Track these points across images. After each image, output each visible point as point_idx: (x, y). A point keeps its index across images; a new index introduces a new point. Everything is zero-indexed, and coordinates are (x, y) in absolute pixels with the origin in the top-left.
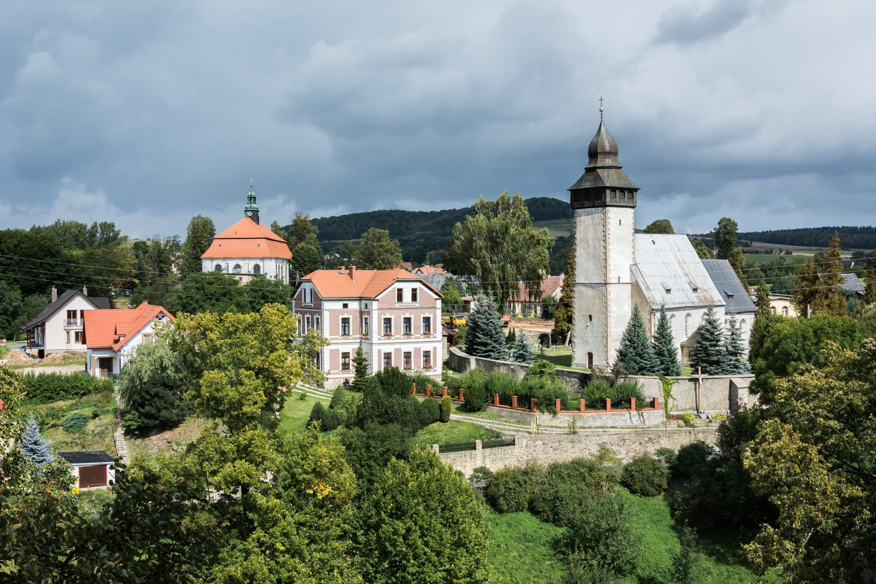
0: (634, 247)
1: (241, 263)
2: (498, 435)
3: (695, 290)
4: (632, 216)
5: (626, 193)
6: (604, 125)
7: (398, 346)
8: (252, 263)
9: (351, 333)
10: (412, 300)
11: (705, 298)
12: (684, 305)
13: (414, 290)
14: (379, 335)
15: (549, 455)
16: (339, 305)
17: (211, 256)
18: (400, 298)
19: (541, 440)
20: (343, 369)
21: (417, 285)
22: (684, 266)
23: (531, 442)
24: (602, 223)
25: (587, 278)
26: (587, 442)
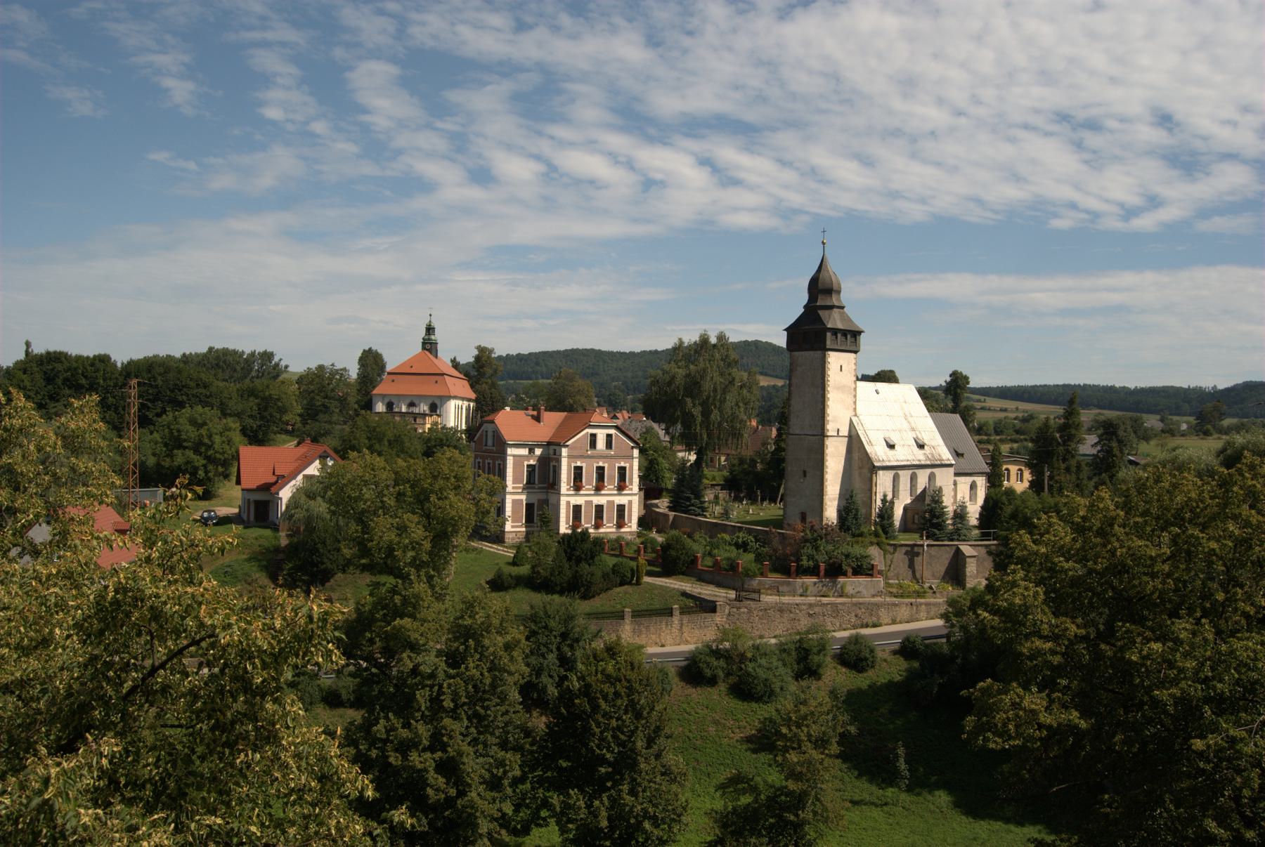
0: (855, 396)
10: (607, 448)
12: (909, 463)
13: (609, 436)
16: (524, 452)
18: (593, 444)
21: (612, 431)
22: (910, 419)
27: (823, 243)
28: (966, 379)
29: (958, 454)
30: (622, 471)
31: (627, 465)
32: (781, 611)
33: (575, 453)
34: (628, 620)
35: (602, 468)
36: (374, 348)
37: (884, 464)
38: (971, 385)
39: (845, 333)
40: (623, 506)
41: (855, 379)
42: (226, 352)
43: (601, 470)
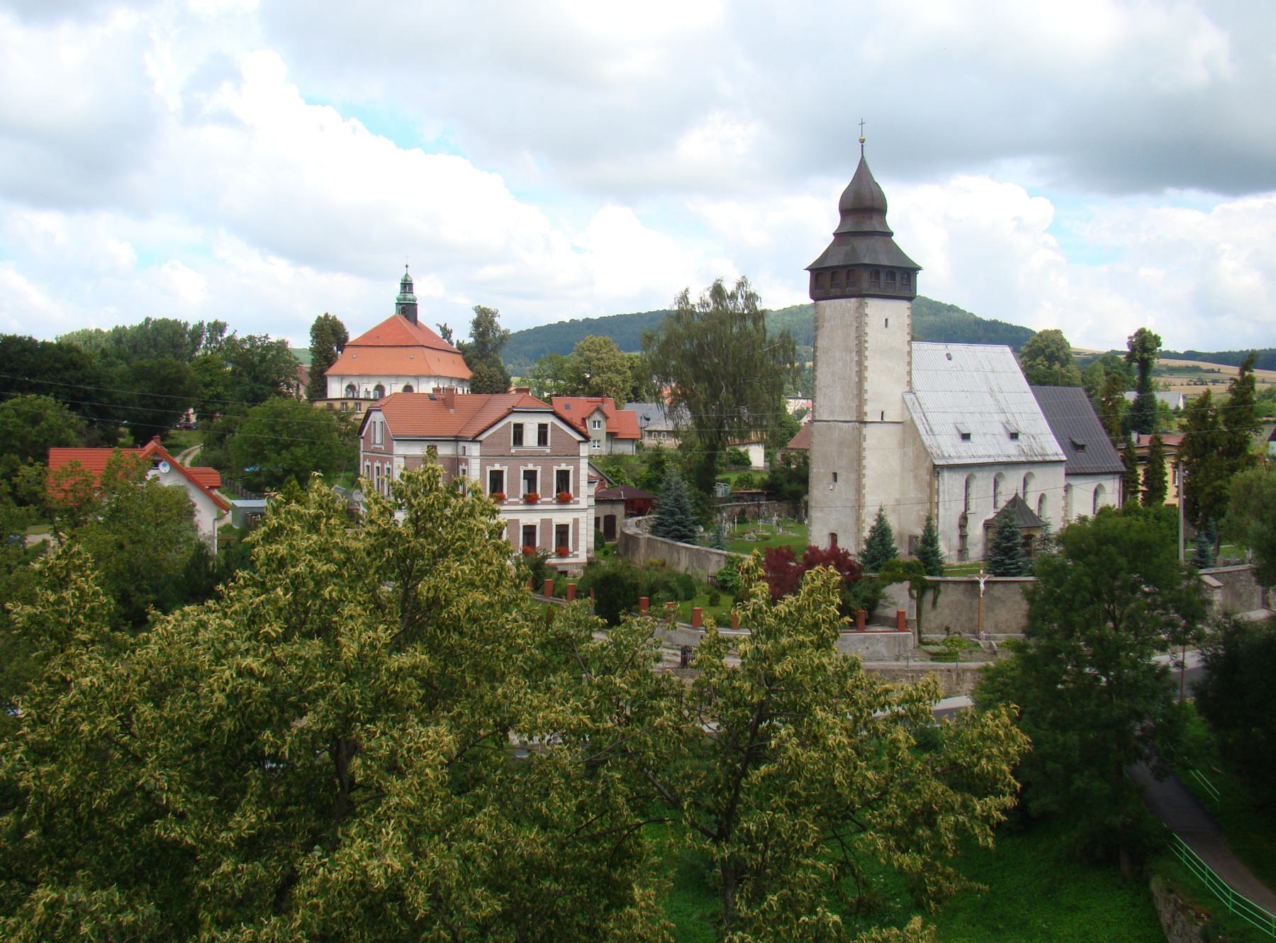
0: (910, 364)
1: (413, 383)
3: (1014, 436)
4: (908, 312)
7: (546, 516)
10: (539, 443)
11: (1031, 449)
12: (991, 460)
13: (542, 428)
16: (419, 450)
17: (366, 372)
18: (518, 439)
21: (549, 420)
22: (999, 396)
24: (855, 324)
25: (832, 412)
27: (862, 141)
28: (1157, 340)
29: (1075, 447)
30: (563, 477)
31: (571, 468)
33: (491, 451)
36: (331, 314)
37: (951, 462)
38: (1163, 348)
40: (533, 527)
41: (909, 338)
42: (165, 324)
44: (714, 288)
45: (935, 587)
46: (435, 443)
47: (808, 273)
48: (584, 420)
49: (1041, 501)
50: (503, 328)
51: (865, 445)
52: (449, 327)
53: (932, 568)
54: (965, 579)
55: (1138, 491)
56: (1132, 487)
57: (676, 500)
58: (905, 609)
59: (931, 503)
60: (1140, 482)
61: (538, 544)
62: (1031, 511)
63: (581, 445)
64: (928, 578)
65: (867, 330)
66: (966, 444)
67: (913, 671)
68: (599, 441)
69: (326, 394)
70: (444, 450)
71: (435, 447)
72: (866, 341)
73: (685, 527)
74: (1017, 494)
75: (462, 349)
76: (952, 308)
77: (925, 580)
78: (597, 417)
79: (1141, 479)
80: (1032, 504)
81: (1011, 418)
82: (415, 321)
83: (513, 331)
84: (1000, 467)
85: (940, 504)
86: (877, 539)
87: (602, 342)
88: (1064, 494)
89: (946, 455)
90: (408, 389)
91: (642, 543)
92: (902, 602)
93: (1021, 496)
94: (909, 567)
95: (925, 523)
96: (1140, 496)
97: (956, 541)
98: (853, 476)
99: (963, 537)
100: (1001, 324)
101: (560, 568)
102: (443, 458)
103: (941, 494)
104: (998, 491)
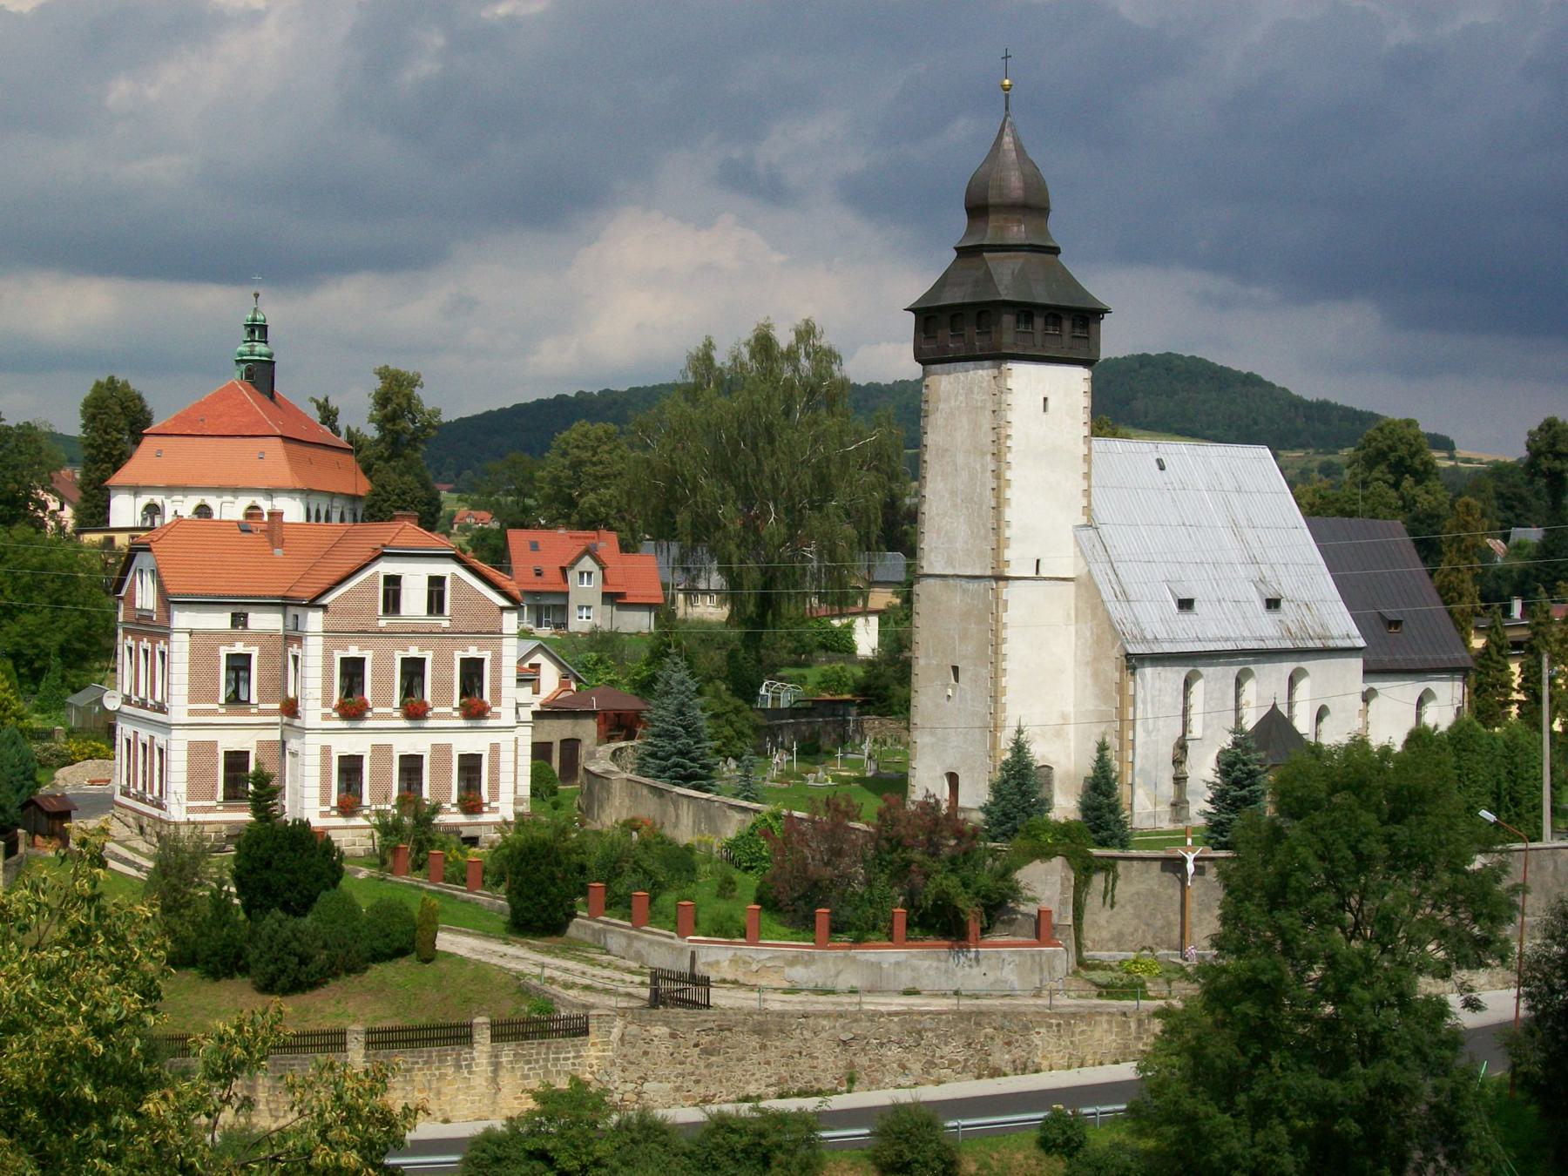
0: (1087, 476)
1: (212, 501)
2: (547, 1006)
3: (1273, 604)
4: (1086, 387)
5: (1039, 322)
6: (1013, 131)
7: (442, 739)
8: (193, 501)
9: (254, 699)
10: (430, 611)
11: (1303, 627)
12: (1230, 646)
13: (436, 583)
14: (325, 705)
15: (688, 1068)
16: (220, 620)
17: (231, 482)
18: (392, 602)
19: (667, 1024)
20: (227, 798)
21: (447, 569)
22: (1249, 534)
23: (633, 1029)
24: (990, 406)
25: (950, 561)
26: (807, 1035)
30: (472, 671)
31: (487, 656)
32: (761, 1030)
33: (345, 624)
34: (483, 1038)
35: (479, 663)
37: (1157, 649)
39: (1054, 315)
40: (418, 759)
41: (1086, 431)
43: (413, 670)
44: (757, 339)
45: (1108, 866)
46: (245, 609)
47: (912, 316)
48: (564, 570)
49: (1320, 717)
50: (428, 406)
51: (1005, 618)
52: (333, 404)
53: (1104, 834)
54: (1161, 854)
55: (1512, 702)
56: (1500, 694)
57: (680, 712)
58: (1054, 907)
59: (1122, 721)
60: (1515, 685)
61: (426, 794)
62: (1300, 736)
63: (505, 615)
64: (1096, 852)
65: (1011, 416)
66: (1186, 617)
67: (1061, 1015)
68: (589, 608)
69: (108, 521)
70: (266, 621)
71: (246, 616)
72: (1008, 436)
73: (693, 760)
74: (1274, 706)
75: (355, 445)
76: (1251, 380)
77: (1090, 855)
78: (587, 564)
79: (1517, 681)
80: (1303, 723)
81: (1268, 573)
82: (272, 396)
83: (447, 417)
84: (1246, 658)
85: (1138, 723)
86: (1012, 783)
87: (601, 433)
88: (1361, 705)
89: (1149, 636)
90: (203, 511)
91: (616, 786)
92: (1048, 893)
93: (1283, 709)
94: (1065, 830)
95: (1095, 756)
96: (1514, 710)
97: (1168, 789)
98: (986, 672)
99: (1180, 780)
100: (1335, 407)
101: (466, 832)
102: (259, 635)
103: (1140, 706)
104: (1243, 700)
